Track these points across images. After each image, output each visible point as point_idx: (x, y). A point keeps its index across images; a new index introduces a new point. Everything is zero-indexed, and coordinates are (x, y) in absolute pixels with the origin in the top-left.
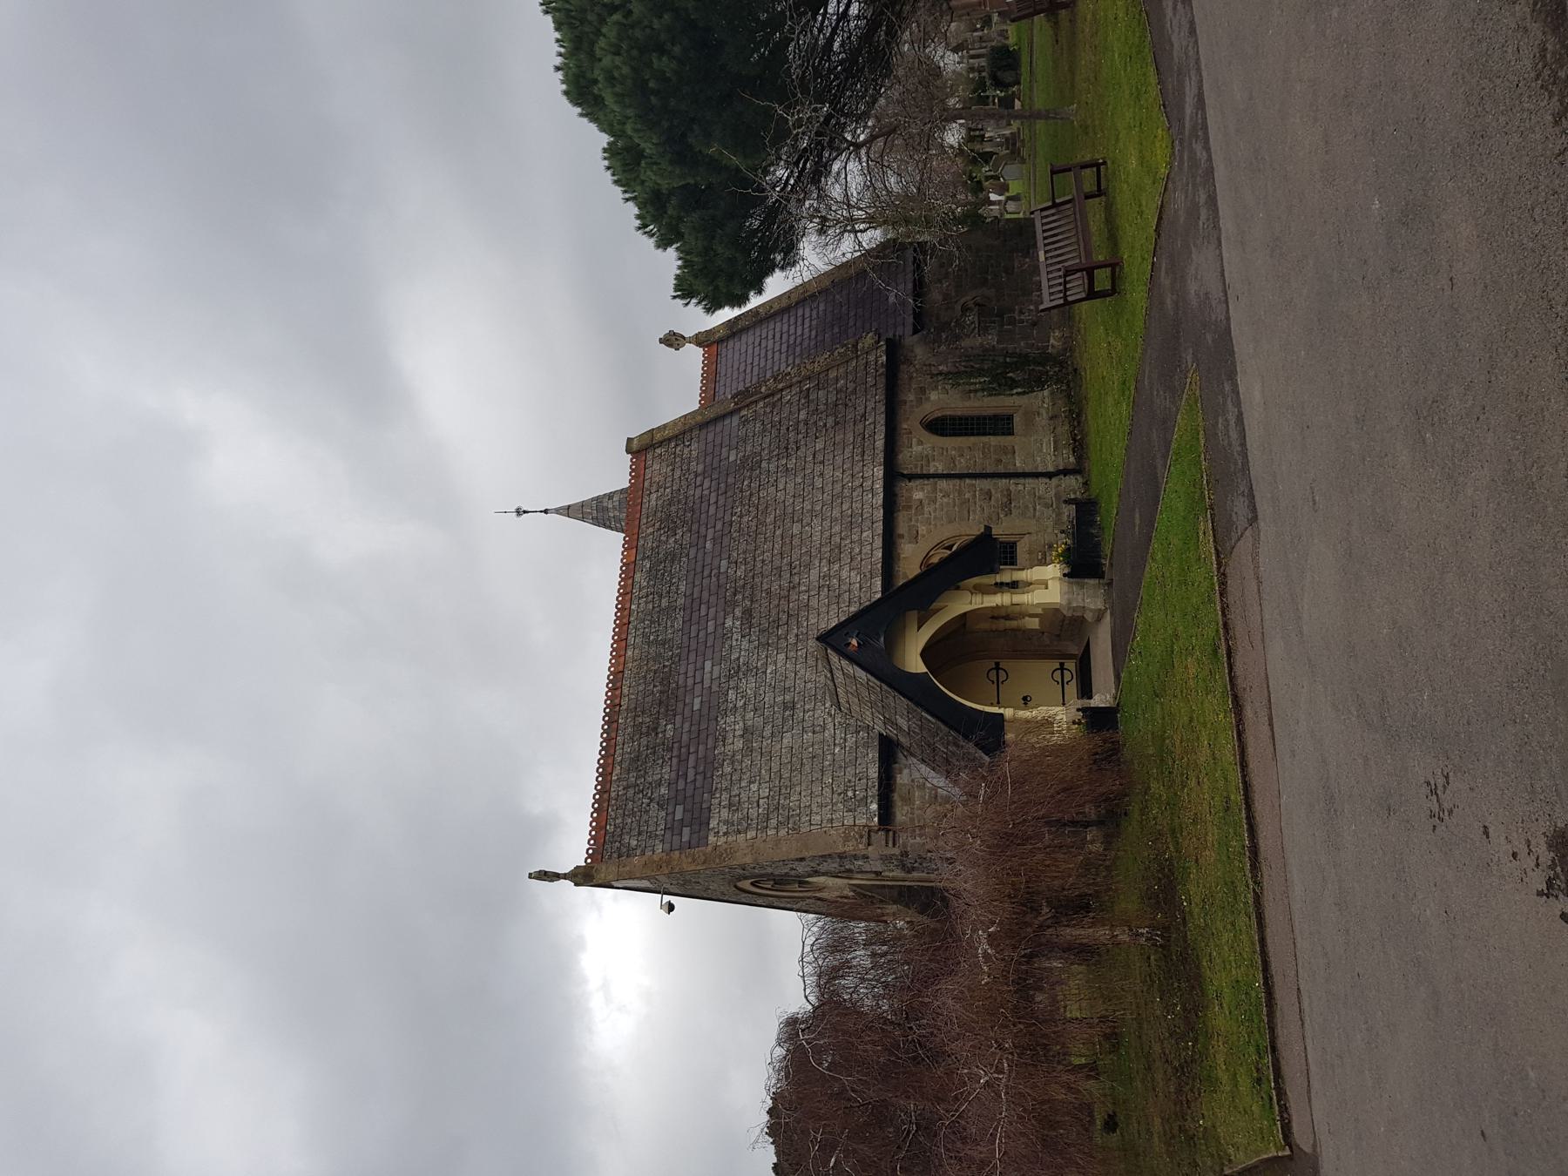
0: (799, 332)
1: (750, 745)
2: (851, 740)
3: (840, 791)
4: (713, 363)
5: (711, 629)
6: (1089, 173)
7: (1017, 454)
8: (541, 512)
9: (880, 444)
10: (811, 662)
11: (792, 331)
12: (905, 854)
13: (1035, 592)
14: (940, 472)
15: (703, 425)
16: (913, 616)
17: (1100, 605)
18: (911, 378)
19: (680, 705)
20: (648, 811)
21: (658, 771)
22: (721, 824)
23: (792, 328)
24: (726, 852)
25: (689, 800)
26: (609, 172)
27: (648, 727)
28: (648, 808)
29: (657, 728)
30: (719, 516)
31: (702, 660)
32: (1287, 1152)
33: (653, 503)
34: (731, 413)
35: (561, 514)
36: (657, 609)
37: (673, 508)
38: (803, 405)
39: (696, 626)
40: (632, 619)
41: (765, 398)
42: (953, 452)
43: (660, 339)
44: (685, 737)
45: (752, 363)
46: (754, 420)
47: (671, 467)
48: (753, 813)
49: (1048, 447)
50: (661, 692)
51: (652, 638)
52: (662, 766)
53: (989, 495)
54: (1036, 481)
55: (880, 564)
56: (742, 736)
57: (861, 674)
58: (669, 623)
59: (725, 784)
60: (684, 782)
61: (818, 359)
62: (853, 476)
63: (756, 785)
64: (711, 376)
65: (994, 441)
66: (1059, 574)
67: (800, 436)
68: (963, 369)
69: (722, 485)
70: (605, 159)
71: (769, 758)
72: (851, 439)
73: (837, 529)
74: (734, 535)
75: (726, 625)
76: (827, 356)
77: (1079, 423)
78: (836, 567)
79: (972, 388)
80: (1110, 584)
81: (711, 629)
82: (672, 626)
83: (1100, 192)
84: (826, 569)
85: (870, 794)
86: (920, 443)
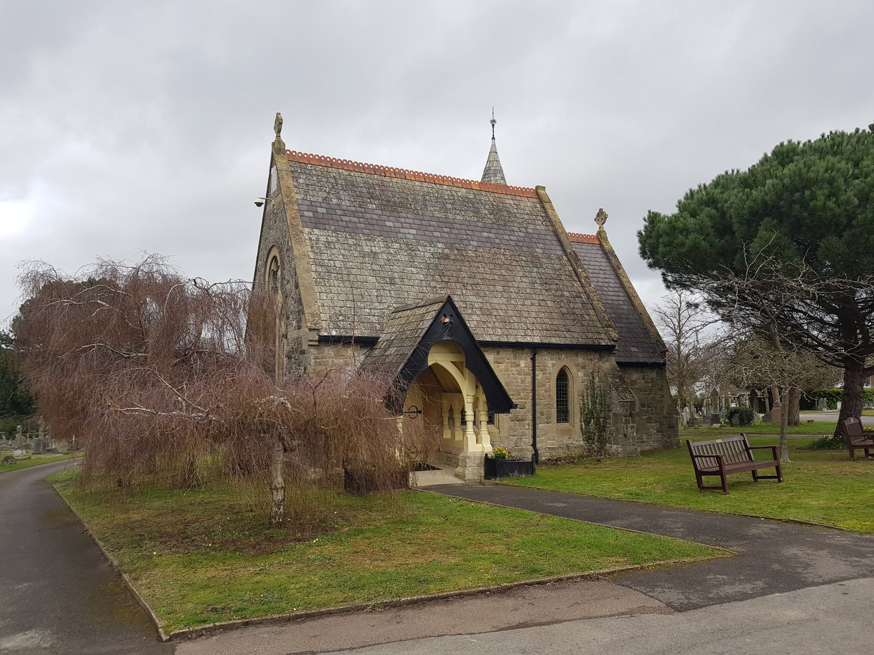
1: (366, 256)
2: (374, 319)
3: (342, 311)
5: (435, 234)
6: (772, 471)
7: (546, 424)
8: (493, 135)
9: (554, 341)
10: (420, 296)
11: (610, 289)
12: (303, 352)
13: (489, 436)
16: (461, 358)
17: (468, 476)
19: (388, 213)
20: (321, 190)
22: (316, 236)
23: (612, 289)
24: (300, 238)
25: (330, 217)
27: (373, 193)
29: (373, 198)
30: (503, 241)
31: (416, 228)
32: (164, 638)
33: (508, 202)
34: (564, 251)
36: (445, 202)
40: (438, 185)
41: (574, 271)
43: (602, 209)
44: (368, 216)
45: (590, 265)
47: (529, 213)
48: (325, 257)
49: (550, 443)
50: (395, 202)
51: (427, 197)
54: (531, 437)
55: (482, 340)
56: (372, 251)
57: (427, 325)
58: (437, 208)
59: (341, 240)
64: (581, 240)
66: (486, 451)
68: (596, 392)
70: (733, 171)
71: (360, 267)
72: (554, 323)
74: (492, 250)
75: (438, 243)
78: (478, 312)
79: (585, 397)
80: (481, 483)
81: (435, 234)
83: (756, 478)
85: (342, 331)
86: (553, 365)
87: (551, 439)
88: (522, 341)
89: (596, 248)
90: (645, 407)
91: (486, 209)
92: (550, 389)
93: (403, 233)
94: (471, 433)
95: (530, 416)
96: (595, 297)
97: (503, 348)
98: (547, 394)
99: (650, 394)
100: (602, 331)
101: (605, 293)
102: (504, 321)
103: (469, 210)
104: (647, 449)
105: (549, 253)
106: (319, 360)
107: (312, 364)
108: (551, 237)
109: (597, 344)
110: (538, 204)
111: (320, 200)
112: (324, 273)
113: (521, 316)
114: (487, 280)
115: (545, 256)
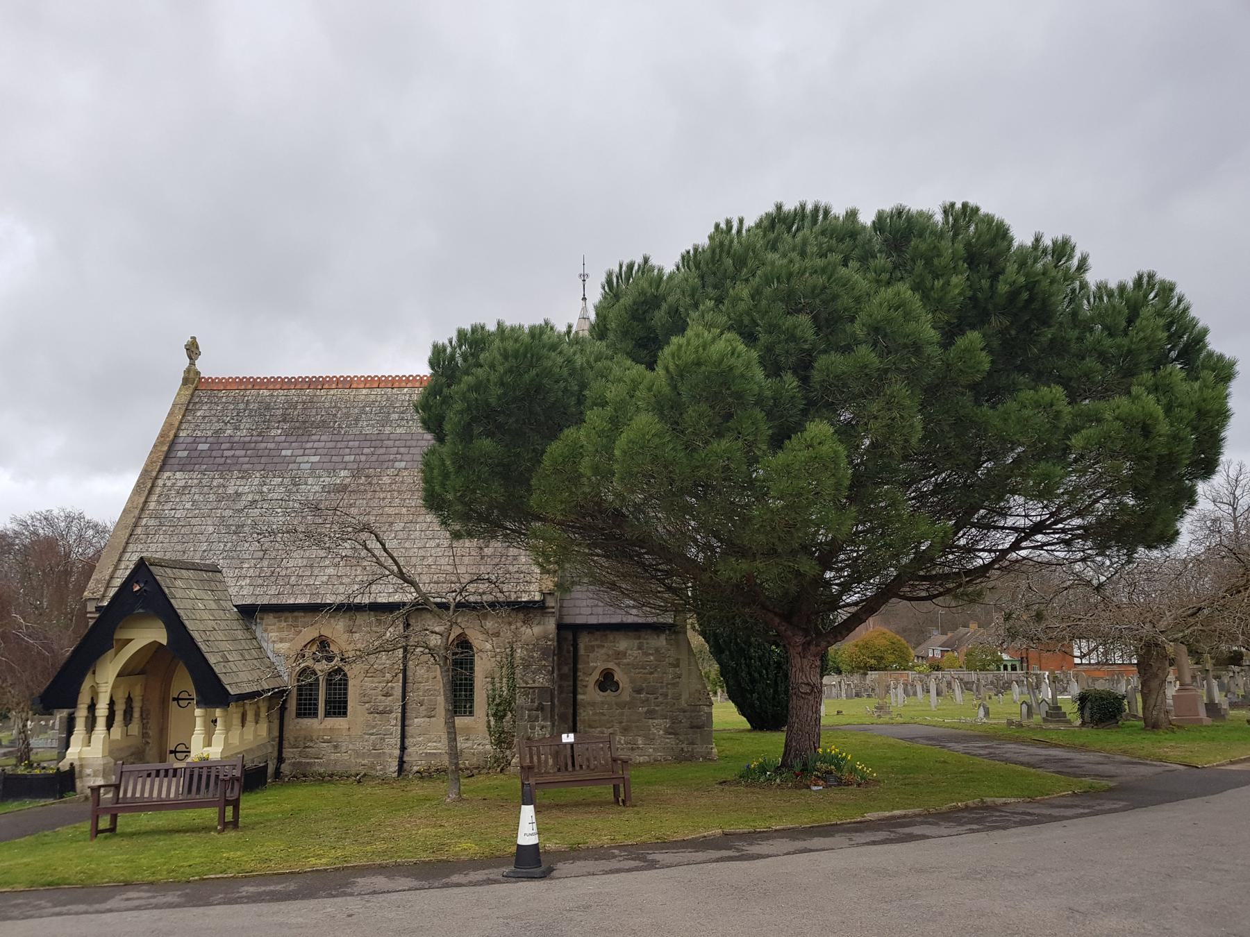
26: (543, 323)
87: (434, 740)
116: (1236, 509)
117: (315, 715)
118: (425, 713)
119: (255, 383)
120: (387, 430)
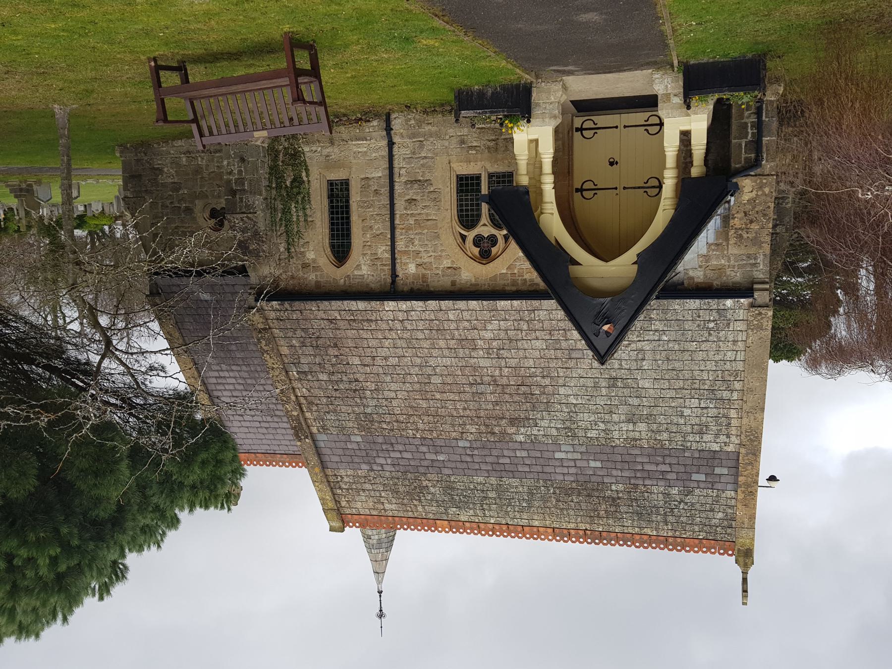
0: (233, 381)
2: (658, 325)
3: (707, 334)
4: (257, 457)
5: (524, 454)
8: (380, 596)
9: (361, 305)
11: (231, 387)
14: (388, 248)
15: (323, 466)
16: (573, 269)
18: (293, 277)
21: (655, 496)
22: (718, 440)
23: (227, 387)
24: (749, 436)
25: (688, 469)
27: (610, 505)
28: (689, 504)
29: (613, 499)
33: (393, 507)
34: (314, 441)
35: (382, 579)
37: (401, 489)
38: (313, 377)
39: (519, 466)
42: (368, 236)
45: (260, 422)
46: (323, 420)
48: (713, 412)
49: (361, 147)
51: (524, 505)
52: (651, 493)
53: (411, 201)
54: (396, 157)
56: (634, 424)
59: (679, 438)
60: (670, 474)
61: (270, 365)
62: (391, 330)
63: (685, 410)
65: (355, 198)
67: (345, 378)
69: (384, 447)
73: (442, 343)
76: (268, 356)
77: (345, 115)
78: (480, 342)
79: (302, 219)
81: (524, 454)
82: (516, 487)
84: (481, 352)
86: (358, 267)
88: (415, 302)
89: (244, 447)
90: (186, 207)
91: (433, 493)
92: (363, 230)
93: (578, 452)
94: (697, 148)
95: (398, 188)
96: (277, 373)
97: (446, 291)
98: (368, 223)
99: (176, 228)
100: (273, 323)
101: (240, 381)
102: (440, 332)
103: (460, 491)
104: (180, 141)
105: (340, 436)
106: (751, 261)
107: (762, 256)
108: (332, 459)
109: (286, 303)
110: (343, 505)
111: (697, 492)
112: (721, 388)
113: (409, 340)
114: (455, 391)
115: (348, 431)
116: (127, 343)
117: (490, 176)
118: (371, 183)
119: (664, 542)
120: (493, 480)
